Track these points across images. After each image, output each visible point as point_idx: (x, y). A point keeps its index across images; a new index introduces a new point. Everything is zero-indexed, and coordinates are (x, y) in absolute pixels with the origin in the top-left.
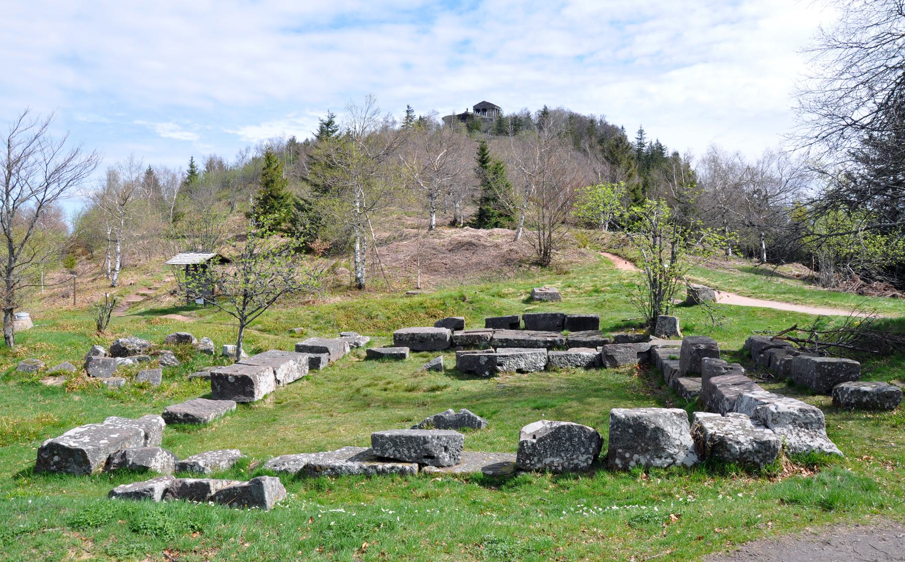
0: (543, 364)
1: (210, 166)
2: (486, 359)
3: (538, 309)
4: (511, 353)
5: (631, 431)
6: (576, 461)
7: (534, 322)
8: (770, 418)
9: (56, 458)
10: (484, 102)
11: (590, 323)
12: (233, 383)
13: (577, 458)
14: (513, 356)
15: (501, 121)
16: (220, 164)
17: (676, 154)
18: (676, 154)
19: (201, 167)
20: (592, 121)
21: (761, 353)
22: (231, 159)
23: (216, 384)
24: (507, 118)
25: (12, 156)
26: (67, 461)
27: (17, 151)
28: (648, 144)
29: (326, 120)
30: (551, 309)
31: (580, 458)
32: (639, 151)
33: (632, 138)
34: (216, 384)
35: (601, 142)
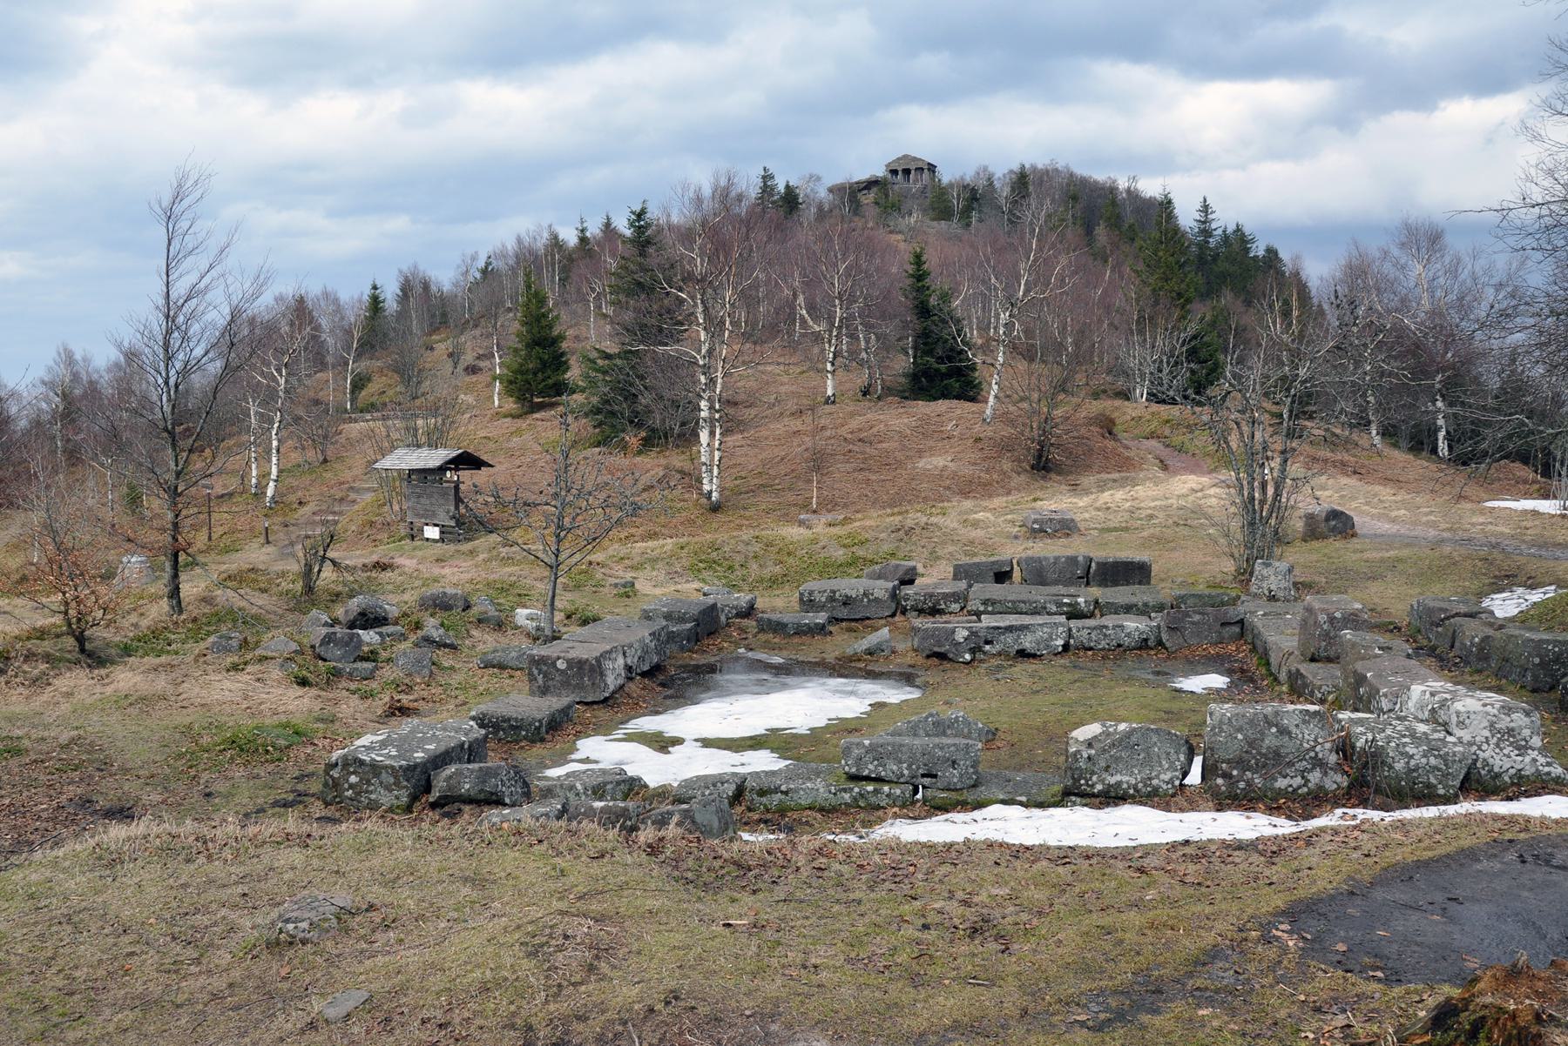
0: (1060, 642)
1: (406, 290)
2: (966, 633)
3: (1050, 549)
4: (1007, 623)
5: (1240, 736)
6: (1155, 782)
7: (1038, 574)
8: (1454, 719)
9: (353, 779)
10: (905, 157)
11: (1134, 573)
12: (562, 671)
13: (1157, 777)
14: (1010, 629)
15: (941, 192)
16: (426, 286)
17: (1272, 253)
18: (1272, 253)
19: (390, 292)
20: (1112, 190)
21: (1438, 625)
22: (445, 277)
23: (536, 672)
24: (951, 185)
25: (173, 296)
26: (368, 782)
27: (180, 289)
28: (1219, 232)
29: (638, 208)
30: (1076, 548)
31: (1162, 777)
32: (1203, 246)
33: (1187, 216)
34: (536, 672)
35: (1105, 222)
